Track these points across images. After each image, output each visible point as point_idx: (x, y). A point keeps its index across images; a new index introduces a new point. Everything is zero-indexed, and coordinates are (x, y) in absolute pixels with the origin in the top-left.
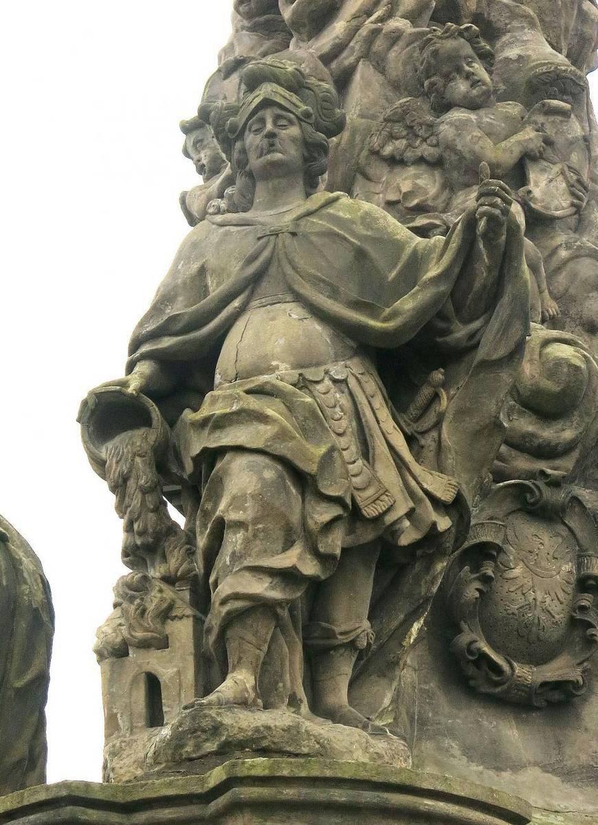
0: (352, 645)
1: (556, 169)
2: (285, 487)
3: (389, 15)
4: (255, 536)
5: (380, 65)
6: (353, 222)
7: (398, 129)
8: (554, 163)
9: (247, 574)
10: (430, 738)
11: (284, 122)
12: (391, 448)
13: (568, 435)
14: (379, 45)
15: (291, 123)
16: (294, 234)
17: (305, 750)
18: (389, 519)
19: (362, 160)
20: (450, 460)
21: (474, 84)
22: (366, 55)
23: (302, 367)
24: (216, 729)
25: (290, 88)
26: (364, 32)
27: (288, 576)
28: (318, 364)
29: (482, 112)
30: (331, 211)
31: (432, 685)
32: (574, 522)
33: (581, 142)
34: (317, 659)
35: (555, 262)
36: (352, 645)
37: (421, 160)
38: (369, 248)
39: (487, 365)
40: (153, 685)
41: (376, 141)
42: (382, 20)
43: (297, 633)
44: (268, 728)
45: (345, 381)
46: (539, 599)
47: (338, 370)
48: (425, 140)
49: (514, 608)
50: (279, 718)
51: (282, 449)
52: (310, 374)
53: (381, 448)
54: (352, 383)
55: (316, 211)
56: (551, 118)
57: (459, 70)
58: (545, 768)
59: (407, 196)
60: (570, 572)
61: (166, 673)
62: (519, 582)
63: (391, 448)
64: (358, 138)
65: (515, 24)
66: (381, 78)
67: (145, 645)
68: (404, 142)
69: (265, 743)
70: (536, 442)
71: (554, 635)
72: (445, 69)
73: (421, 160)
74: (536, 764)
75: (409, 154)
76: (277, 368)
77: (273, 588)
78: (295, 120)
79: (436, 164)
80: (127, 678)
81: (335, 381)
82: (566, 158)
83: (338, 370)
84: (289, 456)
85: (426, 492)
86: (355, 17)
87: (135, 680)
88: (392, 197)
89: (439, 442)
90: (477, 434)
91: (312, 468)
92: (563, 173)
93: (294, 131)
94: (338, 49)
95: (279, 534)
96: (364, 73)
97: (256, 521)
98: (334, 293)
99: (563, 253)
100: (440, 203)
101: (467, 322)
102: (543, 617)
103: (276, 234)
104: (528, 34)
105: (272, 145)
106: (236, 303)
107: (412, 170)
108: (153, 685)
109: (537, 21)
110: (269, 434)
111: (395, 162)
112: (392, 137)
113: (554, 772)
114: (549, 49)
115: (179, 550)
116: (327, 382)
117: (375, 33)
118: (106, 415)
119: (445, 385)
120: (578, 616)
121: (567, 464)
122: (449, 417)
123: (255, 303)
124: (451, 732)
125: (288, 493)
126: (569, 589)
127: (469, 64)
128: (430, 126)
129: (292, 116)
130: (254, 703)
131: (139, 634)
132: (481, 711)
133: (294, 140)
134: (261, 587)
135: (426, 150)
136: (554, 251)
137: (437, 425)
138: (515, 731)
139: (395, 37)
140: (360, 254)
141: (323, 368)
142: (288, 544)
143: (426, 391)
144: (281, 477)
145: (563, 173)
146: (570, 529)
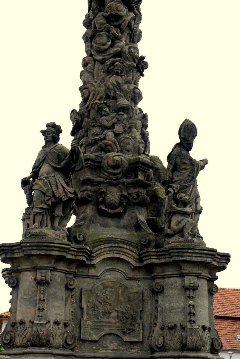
0: (58, 216)
1: (120, 125)
2: (41, 195)
3: (95, 100)
4: (37, 203)
5: (94, 109)
6: (58, 149)
7: (93, 121)
8: (120, 124)
9: (36, 209)
10: (94, 224)
11: (49, 134)
12: (62, 185)
13: (119, 171)
14: (94, 106)
15: (50, 134)
16: (49, 152)
17: (42, 235)
18: (60, 197)
19: (89, 127)
20: (73, 186)
21: (105, 112)
22: (92, 107)
23: (48, 174)
24: (30, 233)
25: (53, 127)
26: (91, 104)
27: (42, 208)
28: (50, 174)
29: (107, 117)
30: (56, 148)
31: (97, 214)
32: (120, 186)
33: (127, 119)
34: (53, 219)
35: (121, 140)
36: (58, 216)
37: (98, 126)
38: (60, 154)
39: (77, 171)
40: (28, 224)
41: (90, 124)
42: (93, 101)
43: (49, 215)
44: (36, 232)
45: (54, 176)
46: (113, 199)
47: (53, 174)
48: (98, 122)
49: (109, 201)
50: (44, 230)
51: (40, 189)
52: (49, 176)
53: (60, 186)
54: (56, 176)
55: (54, 148)
56: (119, 116)
57: (103, 110)
58: (115, 227)
59: (94, 133)
60: (120, 194)
61: (29, 223)
62: (109, 197)
63: (62, 185)
64: (88, 123)
65: (119, 97)
66: (94, 111)
67: (27, 219)
68: (95, 123)
69: (36, 235)
70: (113, 173)
71: (117, 205)
72: (101, 110)
73: (98, 126)
74: (114, 226)
75: (96, 125)
76: (44, 175)
77: (39, 210)
78: (51, 133)
79: (101, 126)
80: (25, 224)
81: (53, 176)
82: (122, 122)
83: (53, 174)
84: (41, 190)
85: (69, 191)
86: (90, 101)
87: (26, 224)
88: (93, 133)
89: (72, 183)
90: (77, 182)
91: (44, 192)
92: (122, 125)
93: (51, 135)
94: (88, 107)
95: (41, 202)
96: (92, 110)
97: (37, 200)
98: (53, 162)
99: (122, 139)
100: (101, 133)
101: (75, 164)
102: (114, 202)
103: (47, 152)
104: (121, 99)
105: (47, 138)
106: (41, 164)
107: (97, 128)
108: (28, 224)
109: (123, 96)
110: (38, 187)
111: (94, 126)
112: (93, 123)
113: (117, 227)
114: (126, 101)
115: (60, 196)
116: (51, 176)
117: (93, 103)
118: (25, 183)
119: (72, 174)
120: (121, 201)
121: (120, 176)
122: (73, 179)
123: (44, 164)
124: (98, 222)
125: (41, 196)
126: (119, 197)
127: (104, 109)
128: (99, 120)
129: (50, 133)
130: (38, 228)
131: (26, 217)
132: (105, 218)
133: (50, 137)
134: (37, 210)
135: (99, 124)
136: (121, 139)
137: (71, 180)
138: (111, 221)
139: (96, 103)
140: (59, 155)
141: (51, 174)
142: (42, 203)
143: (69, 175)
144: (40, 194)
145: (122, 125)
146: (120, 187)
